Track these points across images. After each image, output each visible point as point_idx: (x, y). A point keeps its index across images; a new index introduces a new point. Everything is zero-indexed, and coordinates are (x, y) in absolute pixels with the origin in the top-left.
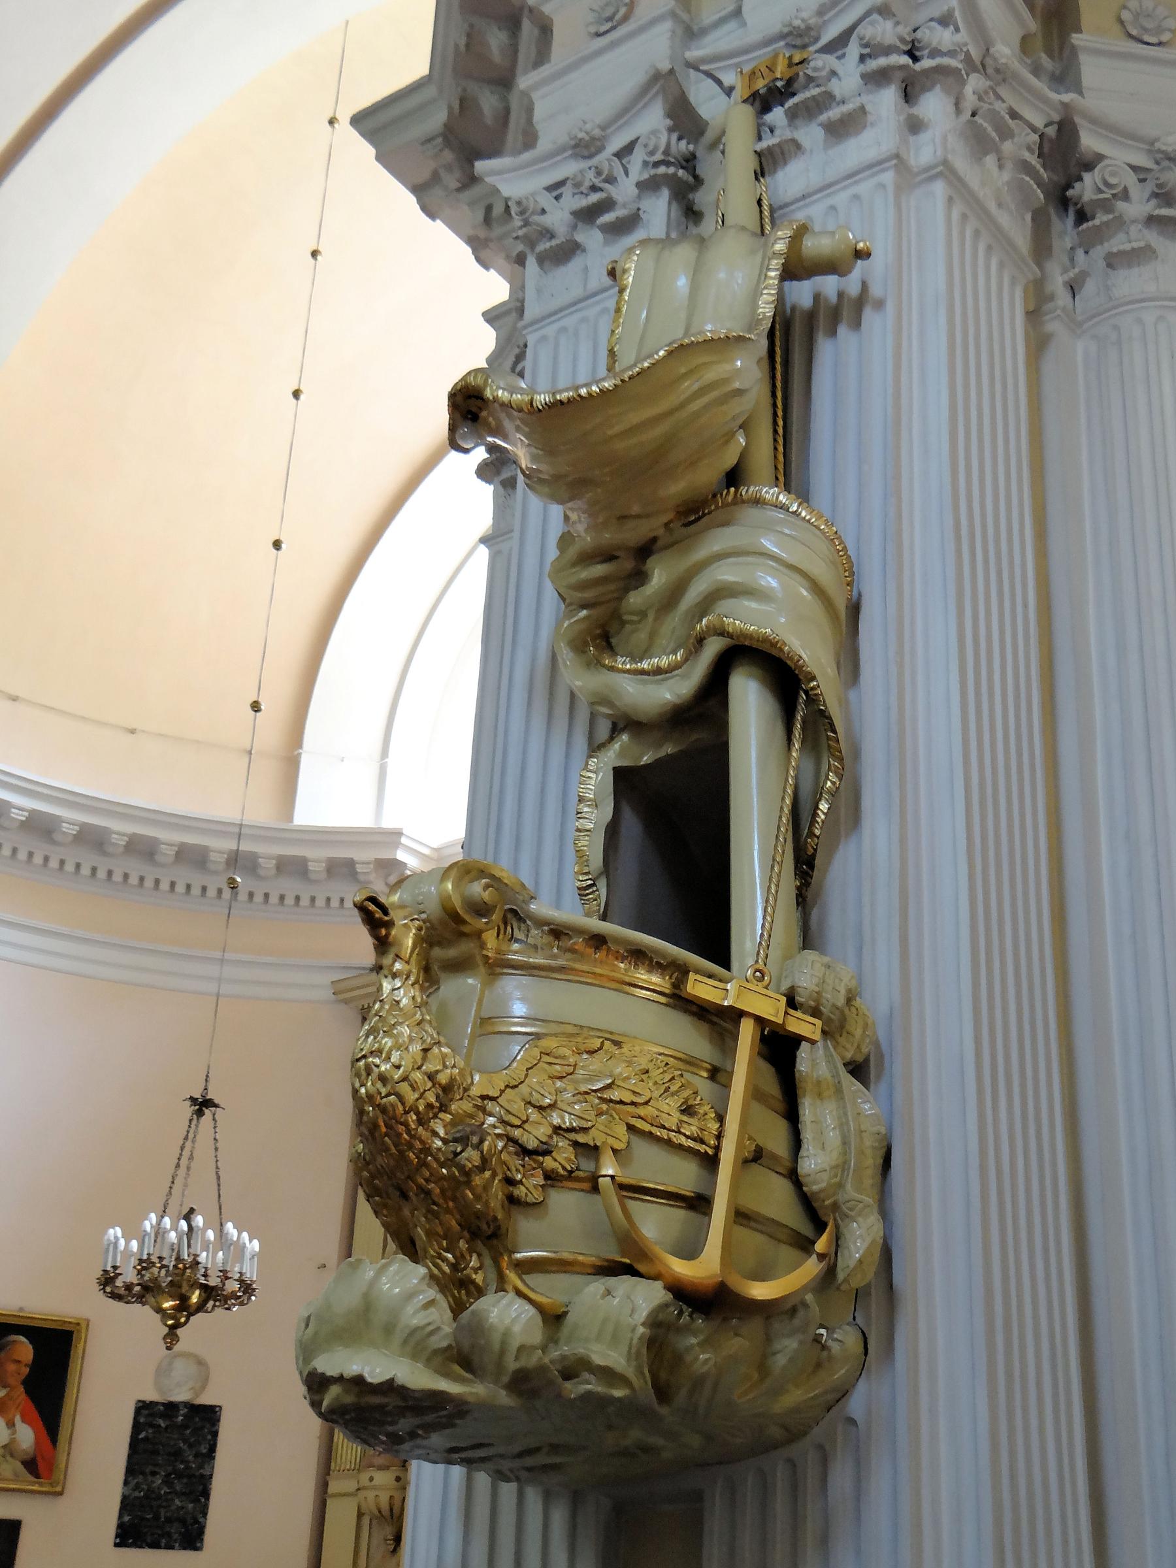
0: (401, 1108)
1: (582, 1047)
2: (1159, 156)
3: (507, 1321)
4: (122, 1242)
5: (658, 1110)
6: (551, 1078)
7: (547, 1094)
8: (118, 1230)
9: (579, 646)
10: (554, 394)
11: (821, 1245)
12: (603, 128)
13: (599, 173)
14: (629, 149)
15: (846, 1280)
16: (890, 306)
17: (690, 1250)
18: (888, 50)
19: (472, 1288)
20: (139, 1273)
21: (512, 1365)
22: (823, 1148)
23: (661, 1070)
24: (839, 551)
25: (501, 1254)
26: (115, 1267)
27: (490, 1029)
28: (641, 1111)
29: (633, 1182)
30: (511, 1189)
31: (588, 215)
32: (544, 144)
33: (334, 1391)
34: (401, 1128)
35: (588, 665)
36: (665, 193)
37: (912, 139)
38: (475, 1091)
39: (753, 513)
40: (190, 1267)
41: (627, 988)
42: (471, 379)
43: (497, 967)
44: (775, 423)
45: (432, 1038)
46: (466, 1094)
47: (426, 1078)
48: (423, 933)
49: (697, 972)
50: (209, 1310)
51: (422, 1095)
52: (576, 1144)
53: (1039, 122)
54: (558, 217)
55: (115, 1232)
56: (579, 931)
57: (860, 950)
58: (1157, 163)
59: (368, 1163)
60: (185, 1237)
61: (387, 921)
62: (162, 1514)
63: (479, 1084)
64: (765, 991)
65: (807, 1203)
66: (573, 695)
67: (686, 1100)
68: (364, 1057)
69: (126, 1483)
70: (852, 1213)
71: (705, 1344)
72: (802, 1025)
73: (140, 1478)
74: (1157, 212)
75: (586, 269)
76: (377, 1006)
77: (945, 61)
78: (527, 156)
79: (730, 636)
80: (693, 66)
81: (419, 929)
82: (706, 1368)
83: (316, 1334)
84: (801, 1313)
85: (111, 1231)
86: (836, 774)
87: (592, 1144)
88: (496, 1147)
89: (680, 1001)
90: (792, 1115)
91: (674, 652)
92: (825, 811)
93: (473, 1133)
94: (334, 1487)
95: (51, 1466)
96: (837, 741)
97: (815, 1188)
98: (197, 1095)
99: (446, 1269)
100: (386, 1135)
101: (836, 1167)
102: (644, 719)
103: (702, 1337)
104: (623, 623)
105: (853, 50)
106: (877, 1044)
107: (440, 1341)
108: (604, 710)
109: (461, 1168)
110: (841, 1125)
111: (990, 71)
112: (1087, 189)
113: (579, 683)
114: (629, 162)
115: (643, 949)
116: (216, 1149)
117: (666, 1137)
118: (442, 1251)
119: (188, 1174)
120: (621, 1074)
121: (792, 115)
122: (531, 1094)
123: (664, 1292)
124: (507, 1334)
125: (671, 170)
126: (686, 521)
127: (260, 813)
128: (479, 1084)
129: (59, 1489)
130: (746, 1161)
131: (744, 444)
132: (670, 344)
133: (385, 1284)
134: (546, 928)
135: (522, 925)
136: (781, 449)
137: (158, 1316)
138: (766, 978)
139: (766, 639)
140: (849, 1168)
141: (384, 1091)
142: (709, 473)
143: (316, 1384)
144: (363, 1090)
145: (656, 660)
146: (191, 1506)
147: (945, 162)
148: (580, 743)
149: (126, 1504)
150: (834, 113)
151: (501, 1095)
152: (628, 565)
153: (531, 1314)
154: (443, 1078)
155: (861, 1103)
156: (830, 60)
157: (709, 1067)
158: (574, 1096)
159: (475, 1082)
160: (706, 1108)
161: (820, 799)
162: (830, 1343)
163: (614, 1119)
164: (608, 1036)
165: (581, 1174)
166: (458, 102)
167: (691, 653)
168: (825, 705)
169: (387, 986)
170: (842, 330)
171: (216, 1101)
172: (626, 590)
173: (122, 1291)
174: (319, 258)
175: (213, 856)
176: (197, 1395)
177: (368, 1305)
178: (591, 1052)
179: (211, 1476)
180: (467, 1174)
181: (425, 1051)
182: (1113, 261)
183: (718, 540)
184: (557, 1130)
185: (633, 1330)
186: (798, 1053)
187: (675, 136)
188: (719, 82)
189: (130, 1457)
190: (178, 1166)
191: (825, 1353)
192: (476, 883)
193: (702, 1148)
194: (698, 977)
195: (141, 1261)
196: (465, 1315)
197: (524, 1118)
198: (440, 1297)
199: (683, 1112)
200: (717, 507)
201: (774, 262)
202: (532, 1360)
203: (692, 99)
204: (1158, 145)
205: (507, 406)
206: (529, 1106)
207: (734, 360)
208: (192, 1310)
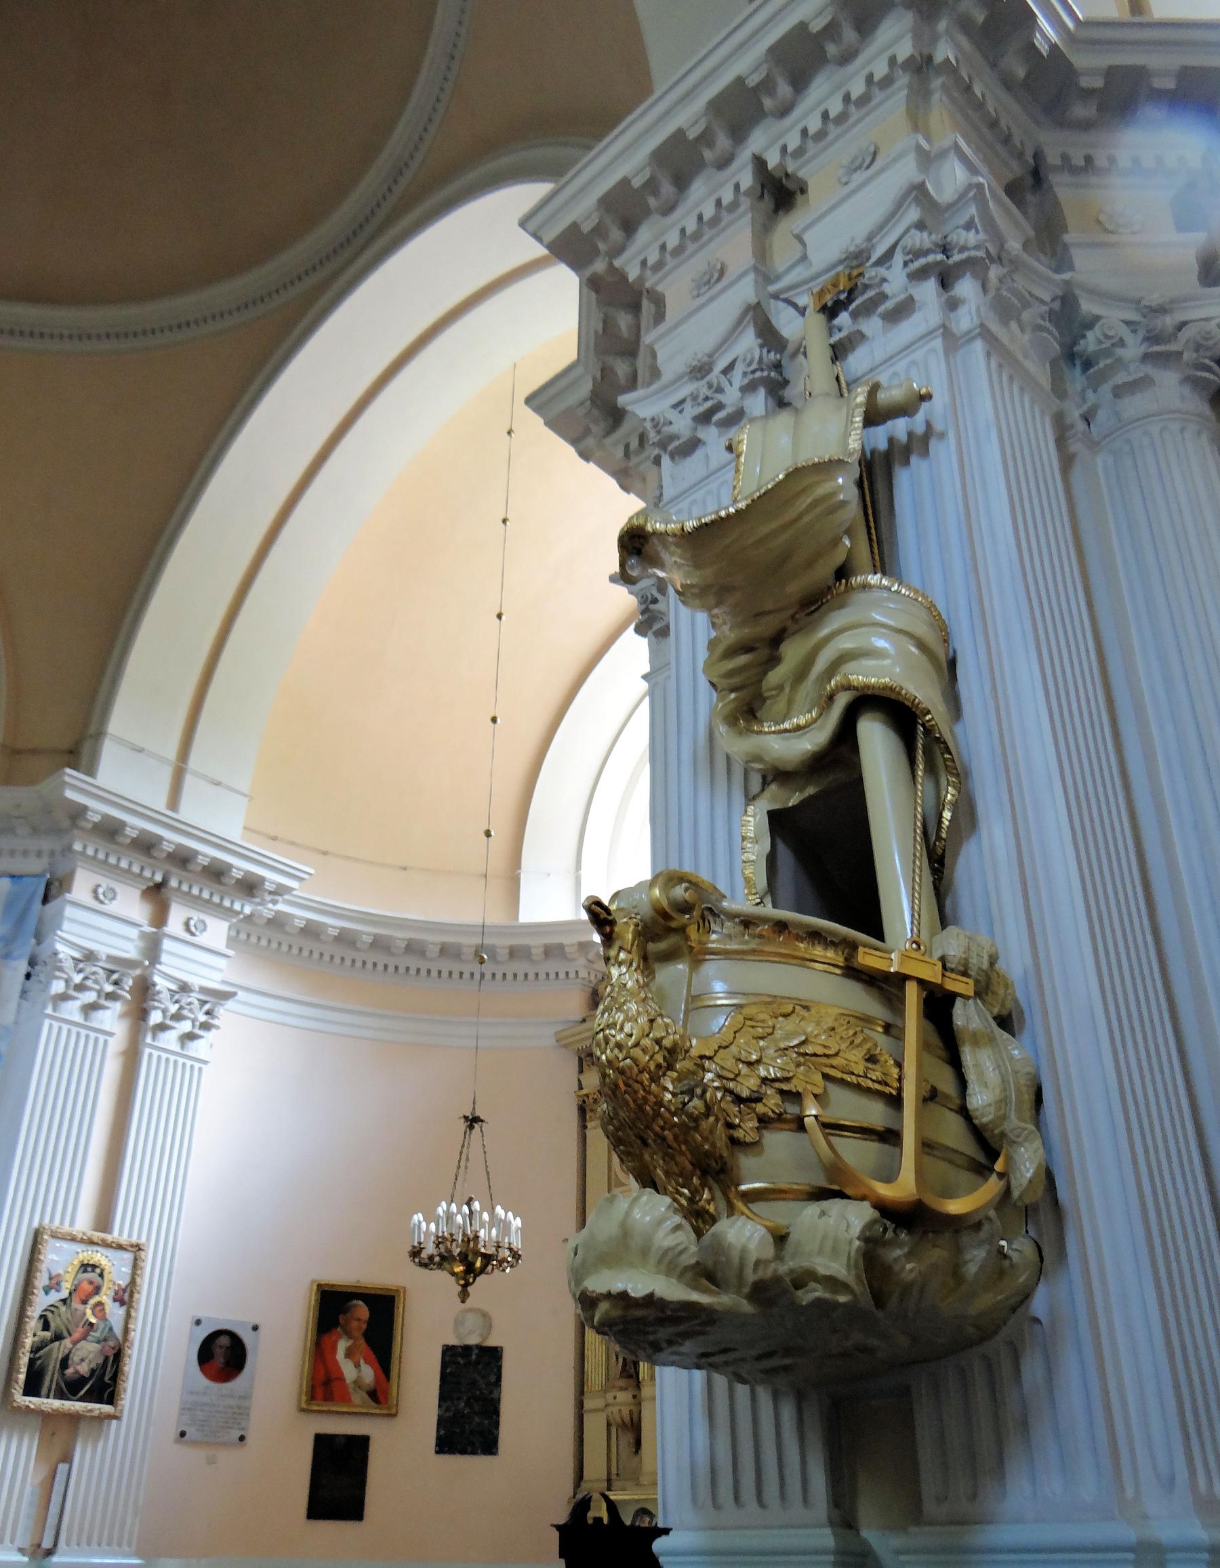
0: (636, 1069)
1: (779, 1012)
2: (1145, 310)
3: (743, 1240)
4: (424, 1225)
5: (846, 1060)
6: (755, 1038)
7: (753, 1052)
8: (420, 1215)
9: (731, 720)
10: (700, 519)
11: (999, 1166)
12: (710, 356)
13: (710, 386)
14: (728, 370)
15: (1020, 1197)
16: (951, 435)
17: (889, 1176)
18: (926, 253)
19: (707, 1216)
20: (437, 1246)
21: (751, 1277)
22: (987, 1087)
23: (845, 1027)
24: (935, 617)
25: (729, 1187)
26: (420, 1243)
27: (700, 1004)
28: (835, 1062)
29: (832, 1121)
30: (731, 1131)
31: (704, 418)
32: (668, 374)
33: (604, 1307)
34: (637, 1086)
35: (740, 733)
36: (762, 392)
37: (952, 315)
38: (694, 1053)
39: (860, 597)
40: (473, 1239)
41: (808, 963)
42: (635, 522)
43: (698, 957)
44: (869, 533)
45: (656, 1011)
46: (687, 1055)
47: (654, 1043)
48: (640, 928)
49: (865, 946)
50: (490, 1271)
51: (651, 1057)
52: (782, 1092)
53: (1047, 297)
54: (682, 425)
55: (418, 1217)
56: (764, 920)
57: (991, 924)
58: (1145, 317)
59: (612, 1119)
60: (468, 1219)
61: (610, 921)
62: (467, 1428)
63: (696, 1047)
64: (922, 958)
65: (978, 1133)
66: (728, 758)
67: (869, 1050)
68: (602, 1030)
69: (440, 1406)
70: (1019, 1140)
71: (910, 1256)
72: (955, 984)
73: (449, 1403)
74: (1150, 350)
75: (707, 457)
76: (609, 989)
77: (973, 253)
78: (655, 387)
79: (856, 688)
80: (776, 296)
81: (637, 925)
82: (913, 1275)
83: (584, 1261)
84: (986, 1227)
85: (415, 1217)
86: (954, 787)
87: (794, 1090)
88: (716, 1097)
89: (853, 972)
90: (955, 1061)
91: (810, 711)
92: (949, 818)
93: (697, 1086)
94: (589, 1404)
95: (386, 1394)
96: (953, 761)
97: (985, 1120)
98: (468, 1114)
99: (684, 1202)
100: (626, 1092)
101: (1000, 1101)
102: (789, 768)
103: (906, 1250)
104: (764, 700)
105: (899, 258)
106: (1016, 1001)
107: (689, 1259)
108: (757, 766)
109: (690, 1116)
110: (999, 1067)
111: (1005, 261)
112: (1090, 342)
113: (735, 749)
114: (732, 376)
115: (819, 931)
116: (485, 1153)
117: (855, 1082)
118: (679, 1188)
119: (466, 1172)
120: (812, 1032)
121: (855, 315)
122: (740, 1052)
123: (872, 1210)
124: (744, 1251)
125: (765, 373)
126: (809, 611)
127: (496, 917)
128: (696, 1047)
129: (393, 1411)
130: (925, 1100)
131: (849, 546)
132: (787, 469)
133: (637, 1214)
134: (737, 920)
135: (718, 920)
136: (876, 551)
137: (453, 1278)
138: (922, 948)
139: (886, 687)
140: (1011, 1102)
141: (621, 1057)
142: (824, 570)
143: (587, 1302)
144: (604, 1057)
145: (795, 720)
146: (486, 1422)
147: (982, 325)
148: (738, 796)
149: (441, 1422)
150: (889, 305)
151: (715, 1054)
152: (763, 653)
153: (763, 1233)
154: (667, 1043)
155: (1012, 1049)
156: (882, 271)
157: (883, 1024)
158: (776, 1051)
159: (693, 1045)
160: (886, 1057)
161: (944, 809)
162: (1011, 1253)
163: (810, 1068)
164: (798, 1002)
165: (788, 1116)
166: (600, 372)
167: (824, 709)
168: (940, 733)
169: (615, 972)
170: (914, 459)
171: (482, 1118)
172: (765, 673)
173: (427, 1261)
174: (508, 523)
175: (465, 950)
176: (485, 1338)
177: (625, 1232)
178: (785, 1016)
179: (499, 1399)
180: (696, 1120)
181: (652, 1021)
182: (1118, 392)
183: (836, 620)
184: (765, 1081)
185: (851, 1242)
186: (954, 1010)
187: (765, 350)
188: (795, 306)
189: (441, 1386)
190: (459, 1167)
191: (1006, 1263)
192: (678, 887)
193: (887, 1090)
194: (867, 950)
195: (438, 1237)
196: (707, 1238)
197: (737, 1072)
198: (684, 1222)
199: (867, 1060)
200: (832, 597)
201: (858, 410)
202: (767, 1273)
203: (774, 322)
204: (1144, 303)
205: (662, 536)
206: (738, 1062)
207: (837, 479)
208: (478, 1271)
